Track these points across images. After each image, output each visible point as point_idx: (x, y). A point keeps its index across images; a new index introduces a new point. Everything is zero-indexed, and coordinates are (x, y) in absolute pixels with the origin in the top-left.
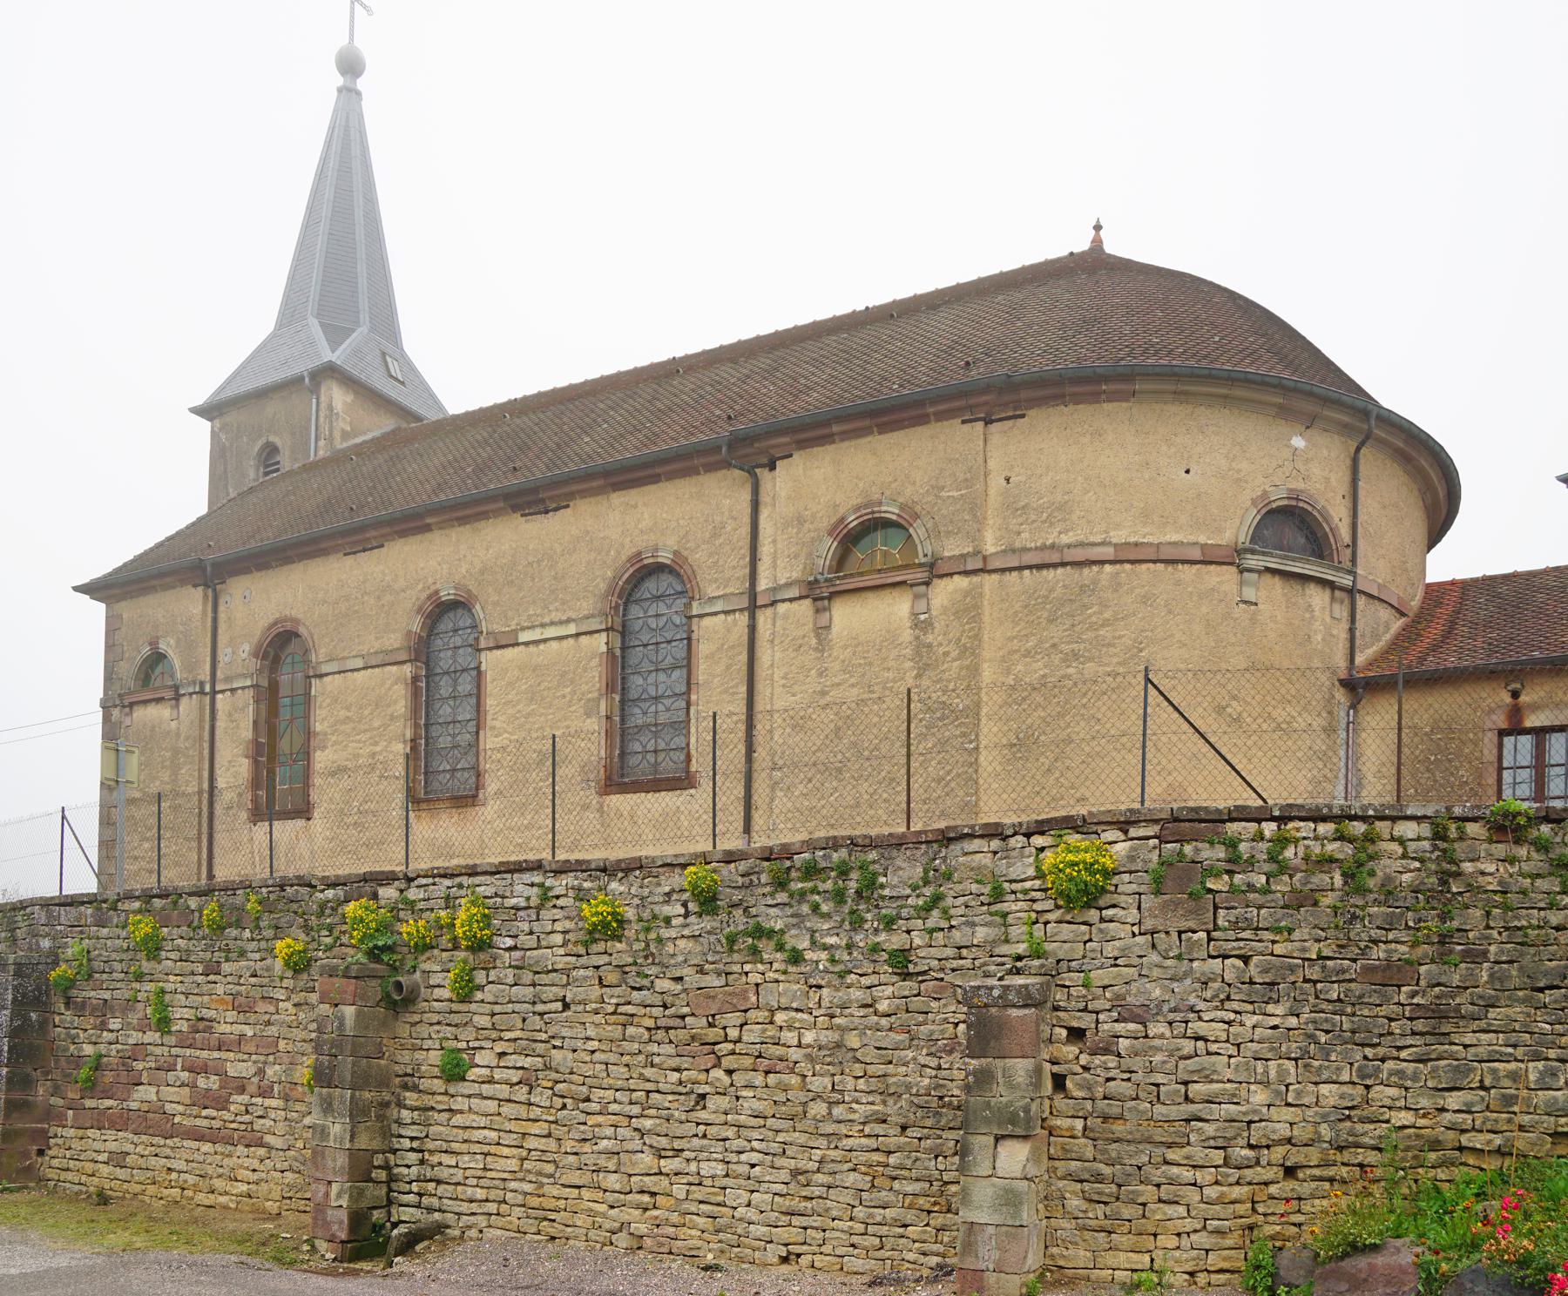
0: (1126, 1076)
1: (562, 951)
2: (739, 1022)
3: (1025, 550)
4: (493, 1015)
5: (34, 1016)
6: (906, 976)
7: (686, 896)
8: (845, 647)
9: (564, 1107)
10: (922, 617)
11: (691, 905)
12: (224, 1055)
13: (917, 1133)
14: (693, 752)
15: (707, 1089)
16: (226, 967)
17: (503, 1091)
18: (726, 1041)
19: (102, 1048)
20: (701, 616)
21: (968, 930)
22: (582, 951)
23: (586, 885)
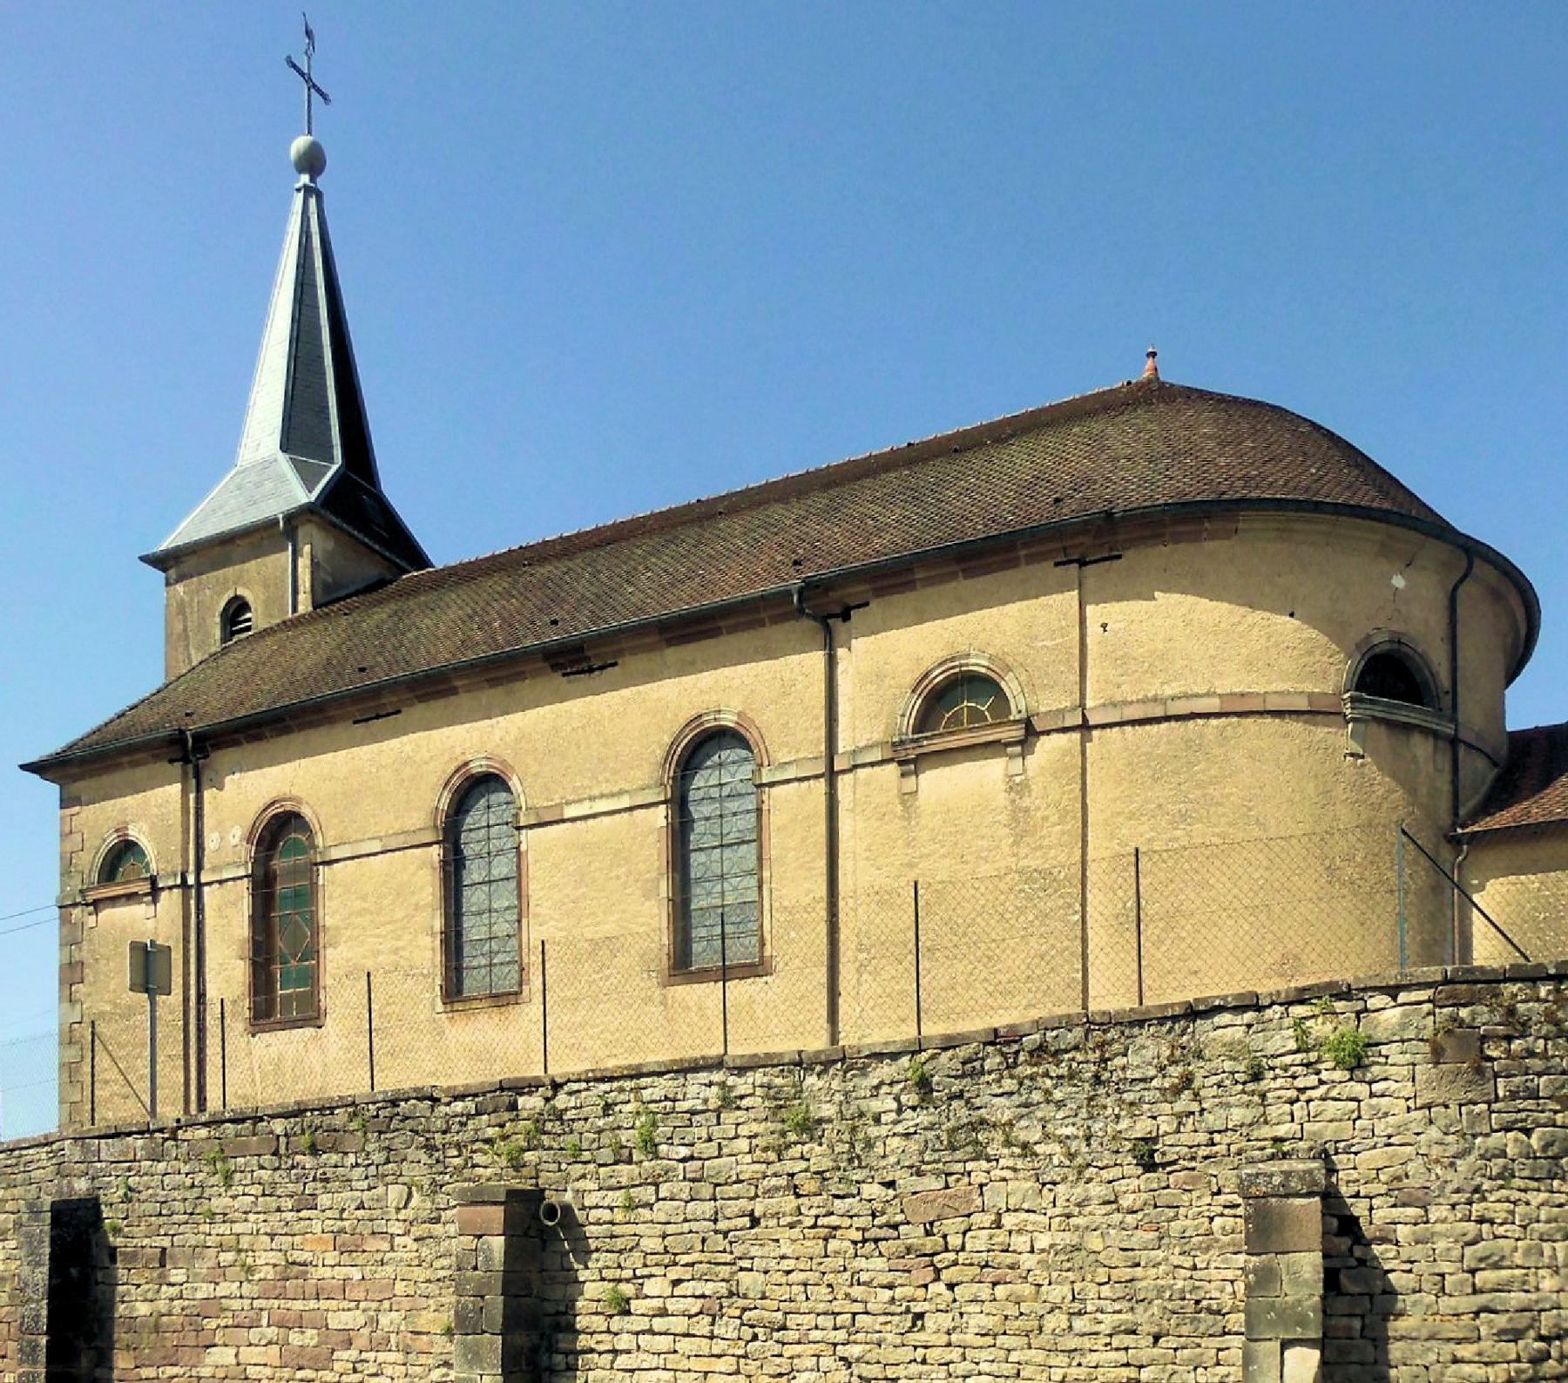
0: (1408, 1266)
1: (748, 1158)
2: (963, 1228)
3: (1125, 703)
4: (664, 1237)
5: (74, 1272)
6: (1150, 1167)
7: (897, 1088)
8: (934, 814)
9: (755, 1337)
10: (1018, 779)
11: (903, 1099)
12: (323, 1304)
13: (1173, 1342)
14: (767, 936)
15: (925, 1306)
16: (324, 1200)
17: (679, 1324)
18: (947, 1250)
19: (162, 1306)
20: (772, 784)
21: (1222, 1112)
22: (772, 1156)
23: (778, 1081)
